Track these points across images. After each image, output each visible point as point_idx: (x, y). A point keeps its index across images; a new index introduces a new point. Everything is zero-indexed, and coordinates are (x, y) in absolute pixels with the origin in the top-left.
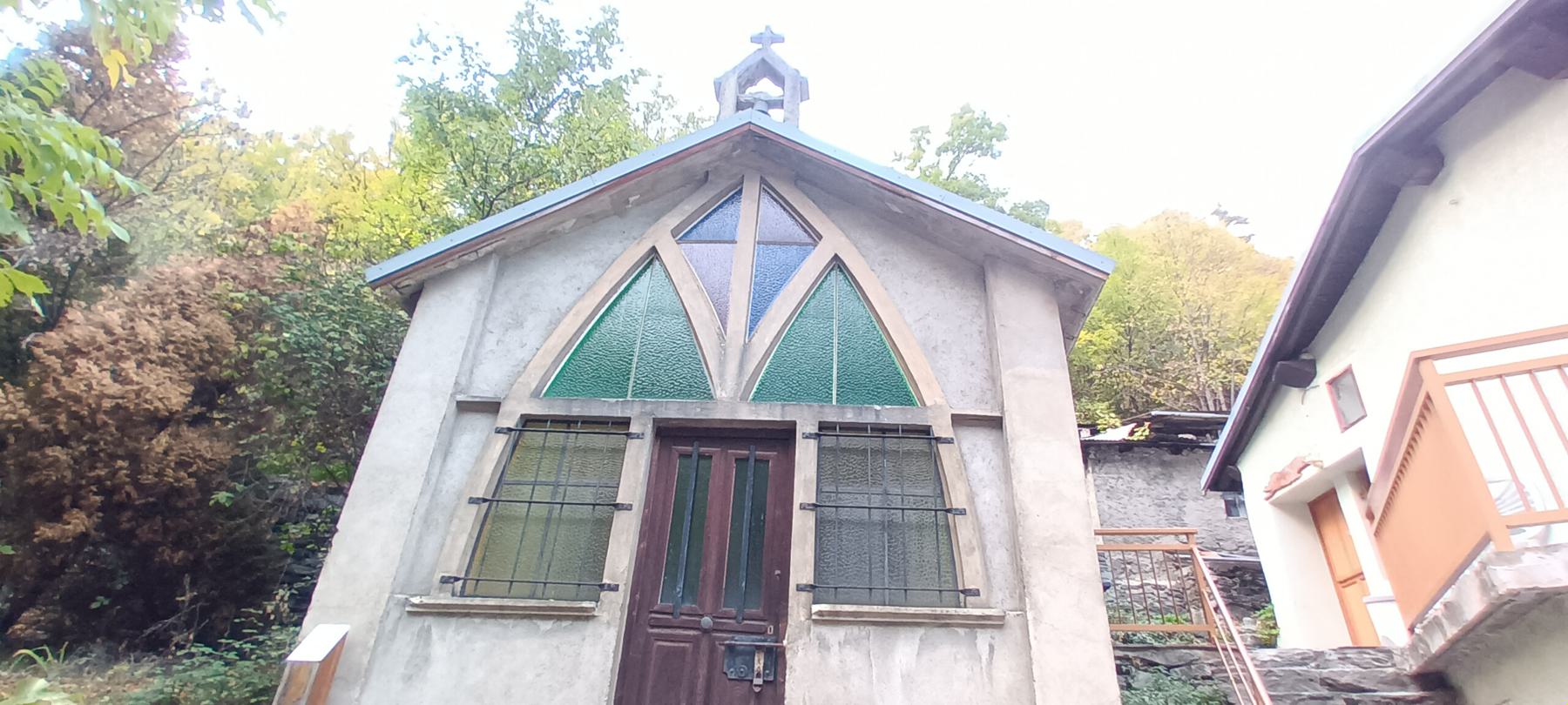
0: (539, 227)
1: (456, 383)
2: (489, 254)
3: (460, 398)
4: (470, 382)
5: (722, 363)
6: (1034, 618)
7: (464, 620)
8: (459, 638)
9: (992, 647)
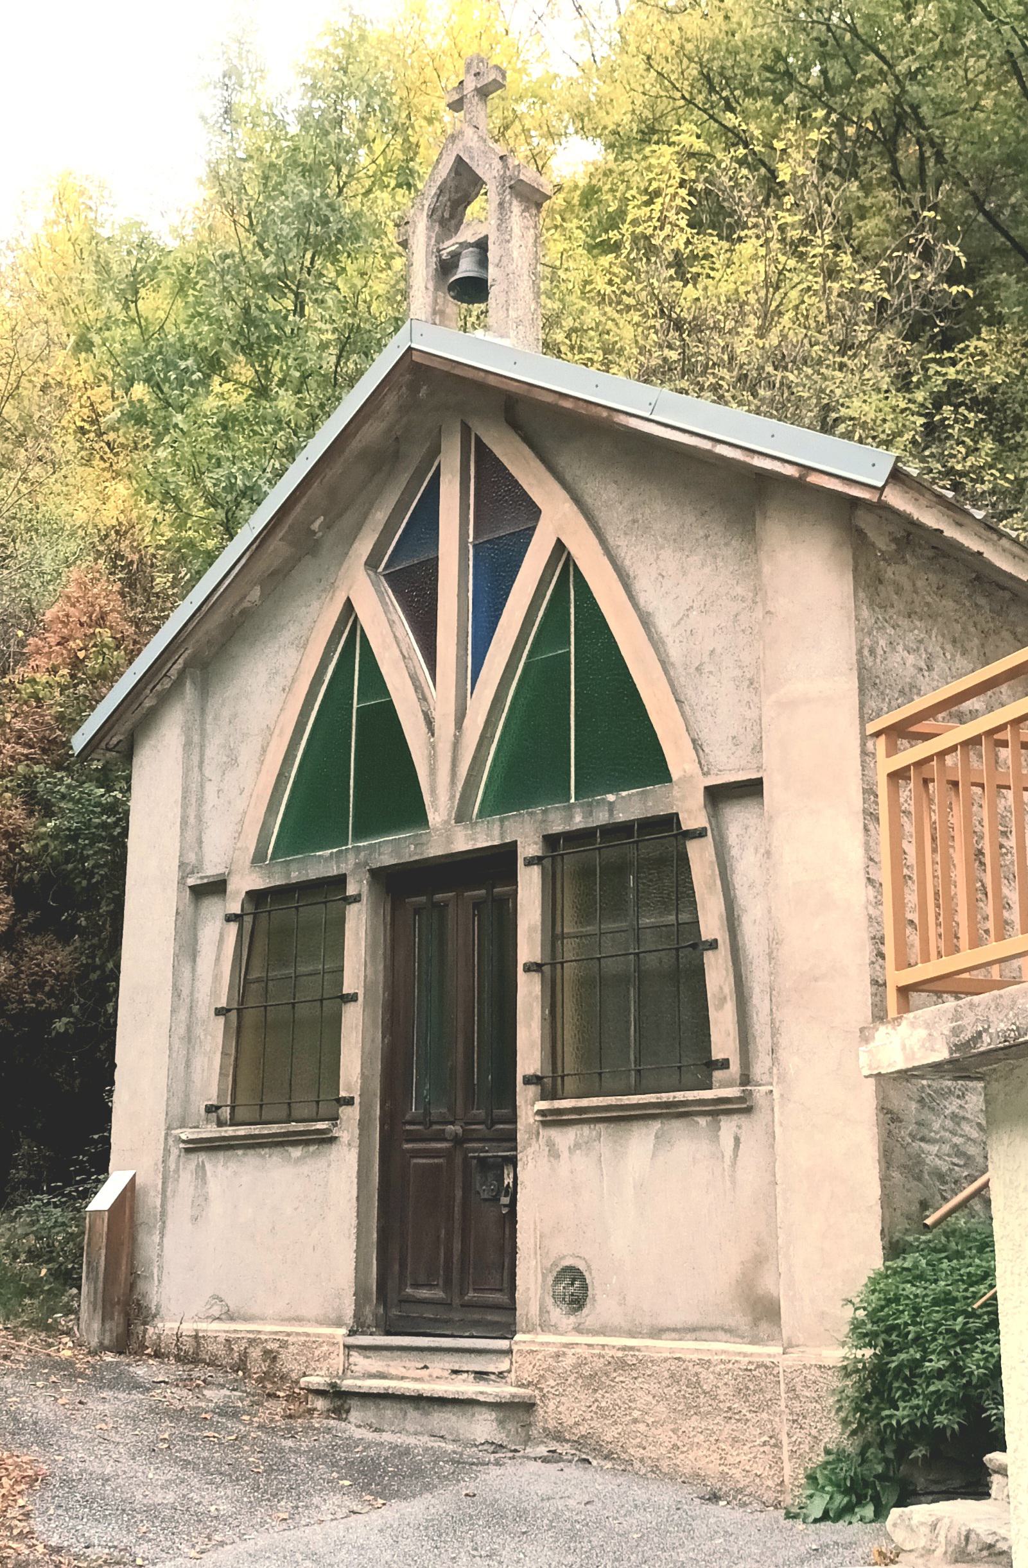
0: (218, 618)
1: (182, 865)
2: (182, 673)
3: (192, 881)
4: (200, 861)
5: (433, 771)
6: (782, 1095)
7: (230, 1153)
8: (229, 1173)
9: (737, 1140)
